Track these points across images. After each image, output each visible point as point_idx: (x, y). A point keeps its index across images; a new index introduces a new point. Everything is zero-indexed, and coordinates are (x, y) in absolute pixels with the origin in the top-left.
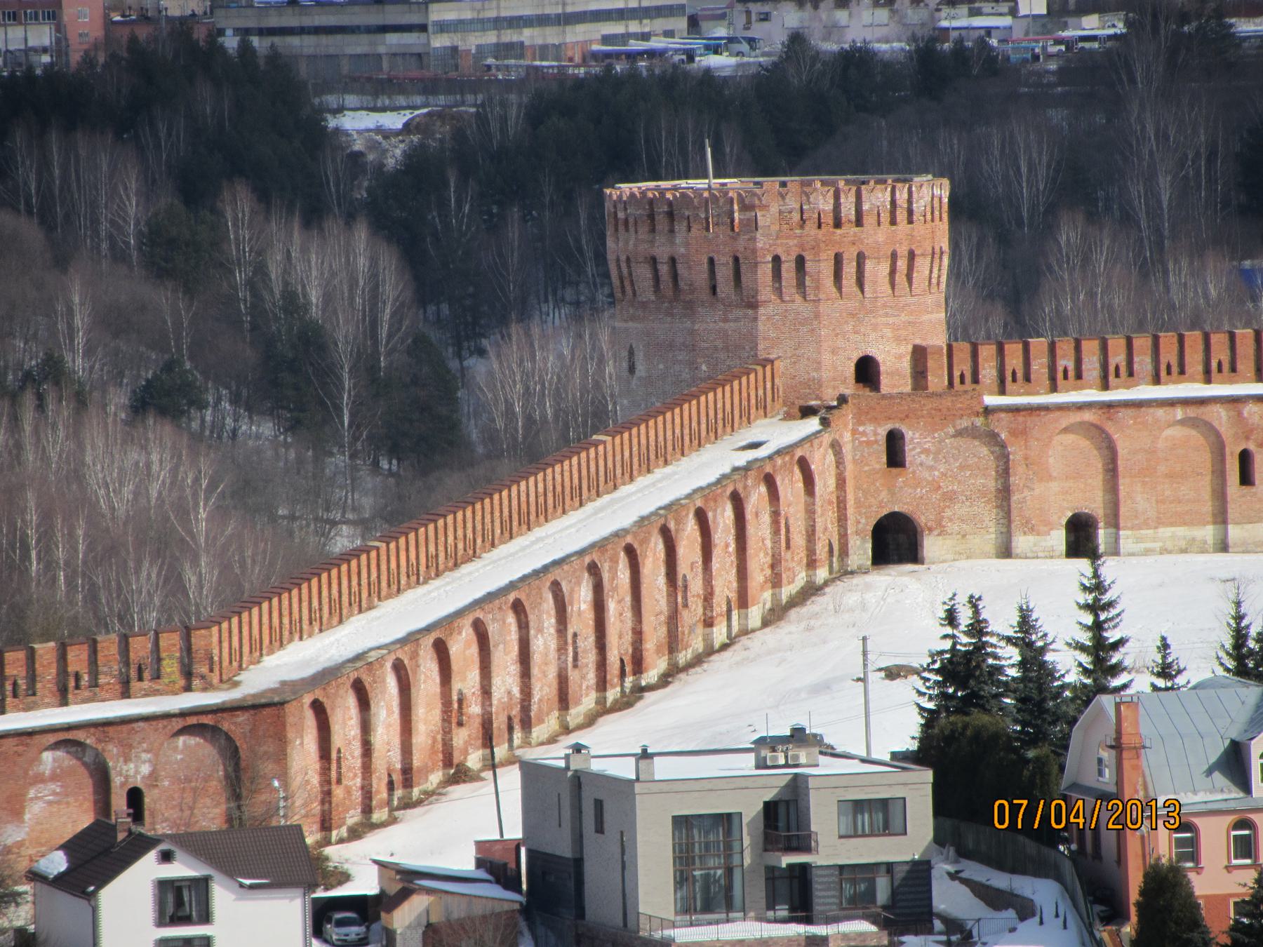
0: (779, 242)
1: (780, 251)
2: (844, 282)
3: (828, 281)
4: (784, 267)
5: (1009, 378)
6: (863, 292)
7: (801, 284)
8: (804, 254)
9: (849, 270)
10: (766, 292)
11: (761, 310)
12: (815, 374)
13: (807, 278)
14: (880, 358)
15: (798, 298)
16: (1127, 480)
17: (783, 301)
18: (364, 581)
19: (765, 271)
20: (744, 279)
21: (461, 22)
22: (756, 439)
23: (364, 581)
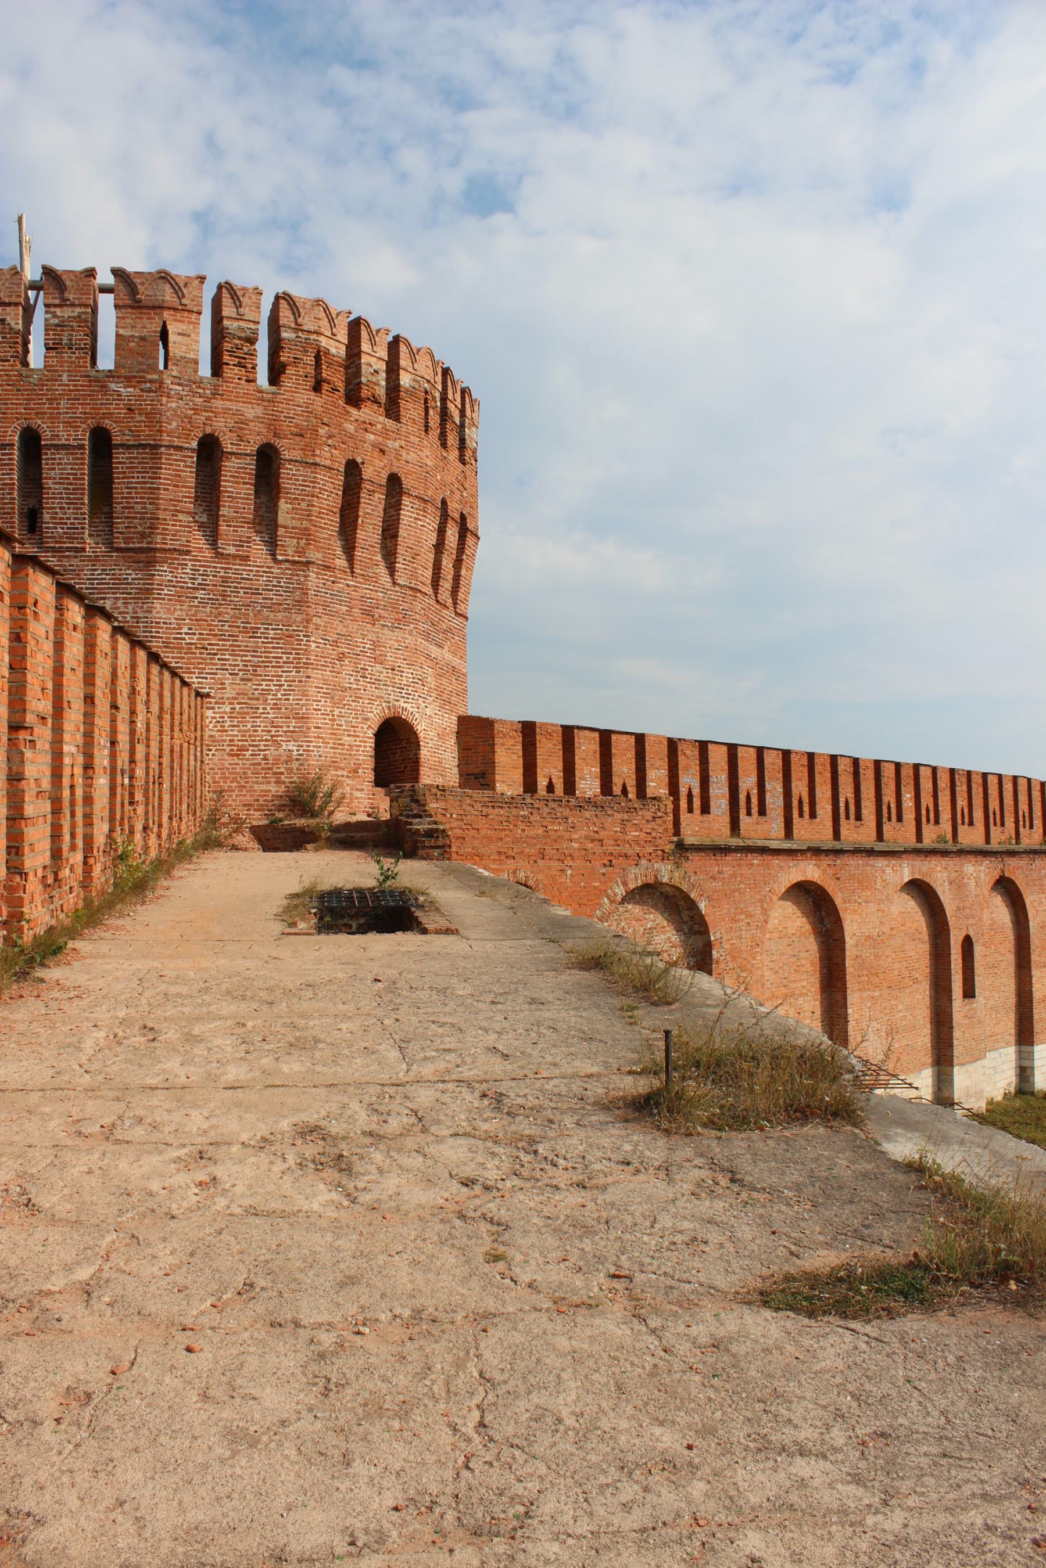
0: (218, 403)
1: (220, 426)
2: (360, 534)
3: (329, 526)
4: (230, 467)
5: (683, 804)
6: (392, 570)
7: (266, 522)
8: (278, 443)
9: (372, 508)
10: (179, 527)
11: (164, 573)
12: (292, 746)
13: (283, 506)
14: (421, 727)
15: (258, 550)
16: (857, 995)
17: (219, 555)
18: (154, 744)
19: (179, 474)
20: (119, 488)
21: (61, 776)
22: (230, 1092)
23: (154, 744)
